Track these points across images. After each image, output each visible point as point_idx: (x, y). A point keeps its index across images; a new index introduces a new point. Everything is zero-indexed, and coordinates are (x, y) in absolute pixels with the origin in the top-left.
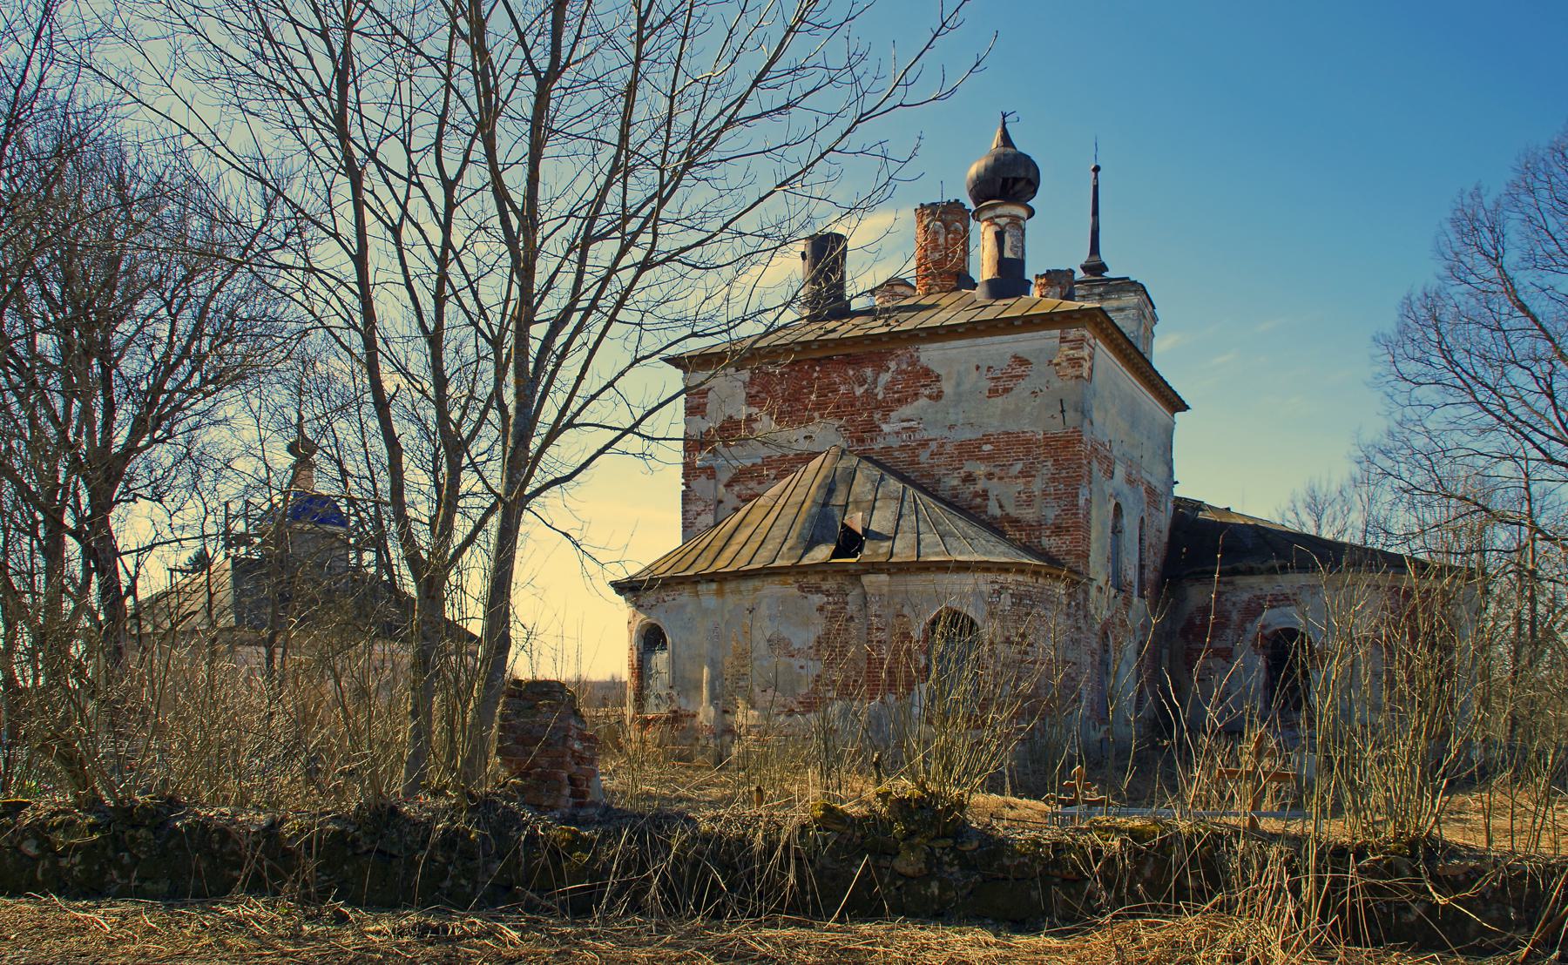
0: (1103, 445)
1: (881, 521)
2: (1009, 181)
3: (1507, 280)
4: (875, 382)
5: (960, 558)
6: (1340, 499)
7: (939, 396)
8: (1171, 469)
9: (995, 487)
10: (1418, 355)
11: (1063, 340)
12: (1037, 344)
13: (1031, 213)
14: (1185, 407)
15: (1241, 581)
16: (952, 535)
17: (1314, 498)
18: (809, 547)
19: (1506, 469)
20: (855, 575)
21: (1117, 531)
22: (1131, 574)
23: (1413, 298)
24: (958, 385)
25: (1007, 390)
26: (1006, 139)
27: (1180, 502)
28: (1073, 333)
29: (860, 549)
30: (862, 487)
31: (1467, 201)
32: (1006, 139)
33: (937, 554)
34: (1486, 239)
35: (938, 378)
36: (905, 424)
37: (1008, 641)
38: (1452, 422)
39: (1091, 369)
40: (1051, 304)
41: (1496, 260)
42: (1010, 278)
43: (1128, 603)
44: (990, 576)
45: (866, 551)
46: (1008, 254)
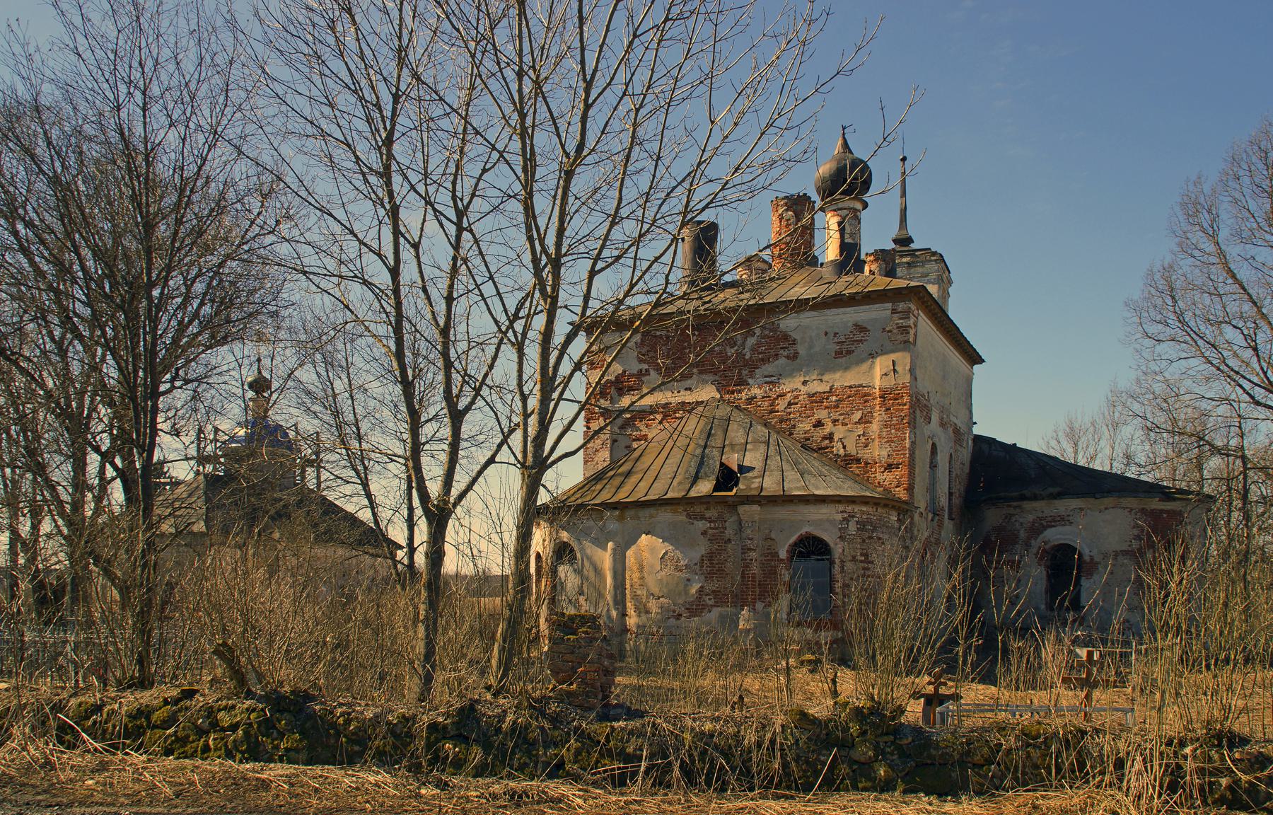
0: (923, 396)
1: (753, 458)
2: (848, 183)
3: (1222, 254)
4: (743, 344)
5: (817, 493)
6: (1092, 429)
7: (794, 357)
8: (971, 412)
9: (839, 432)
10: (1158, 318)
11: (894, 311)
12: (874, 315)
13: (865, 206)
14: (981, 361)
15: (1027, 505)
16: (810, 473)
17: (1072, 429)
18: (695, 479)
19: (1223, 409)
20: (732, 505)
21: (933, 466)
22: (944, 501)
23: (1155, 270)
24: (811, 347)
25: (849, 352)
26: (845, 145)
27: (979, 439)
28: (902, 306)
29: (736, 484)
30: (736, 434)
31: (1191, 188)
32: (845, 145)
33: (798, 489)
34: (1205, 218)
35: (794, 342)
37: (854, 559)
38: (1189, 374)
39: (915, 335)
40: (881, 283)
41: (1213, 237)
42: (850, 257)
43: (941, 525)
44: (841, 507)
45: (741, 486)
46: (848, 240)
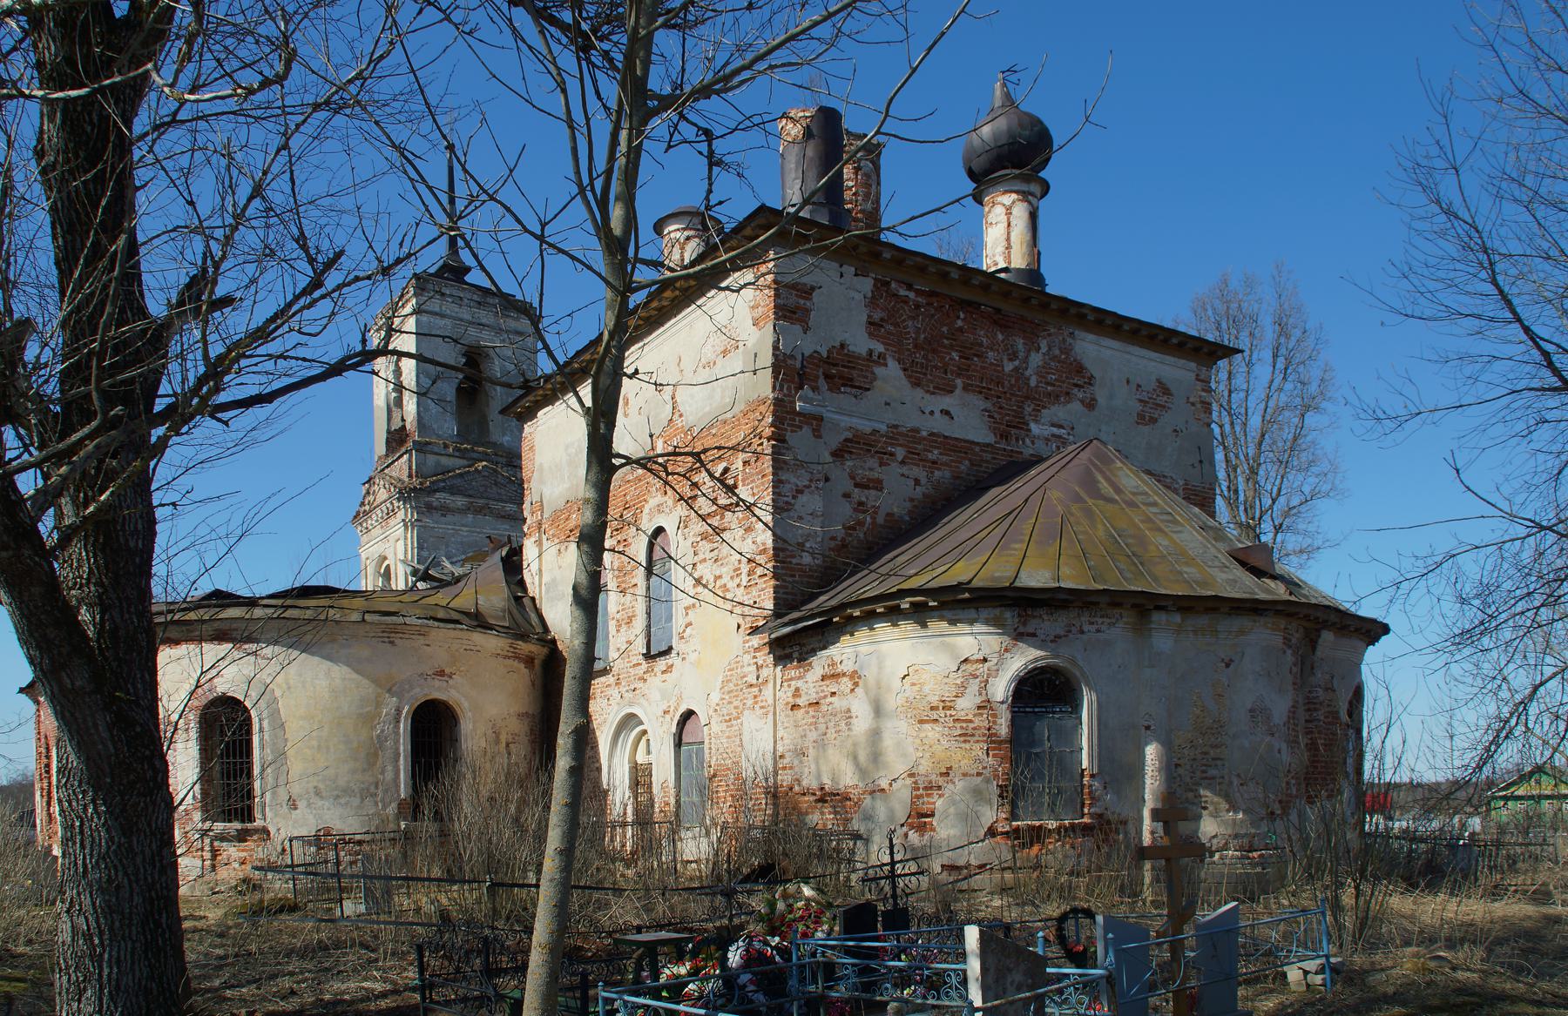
7: (1090, 404)
25: (1153, 421)
36: (1055, 430)
